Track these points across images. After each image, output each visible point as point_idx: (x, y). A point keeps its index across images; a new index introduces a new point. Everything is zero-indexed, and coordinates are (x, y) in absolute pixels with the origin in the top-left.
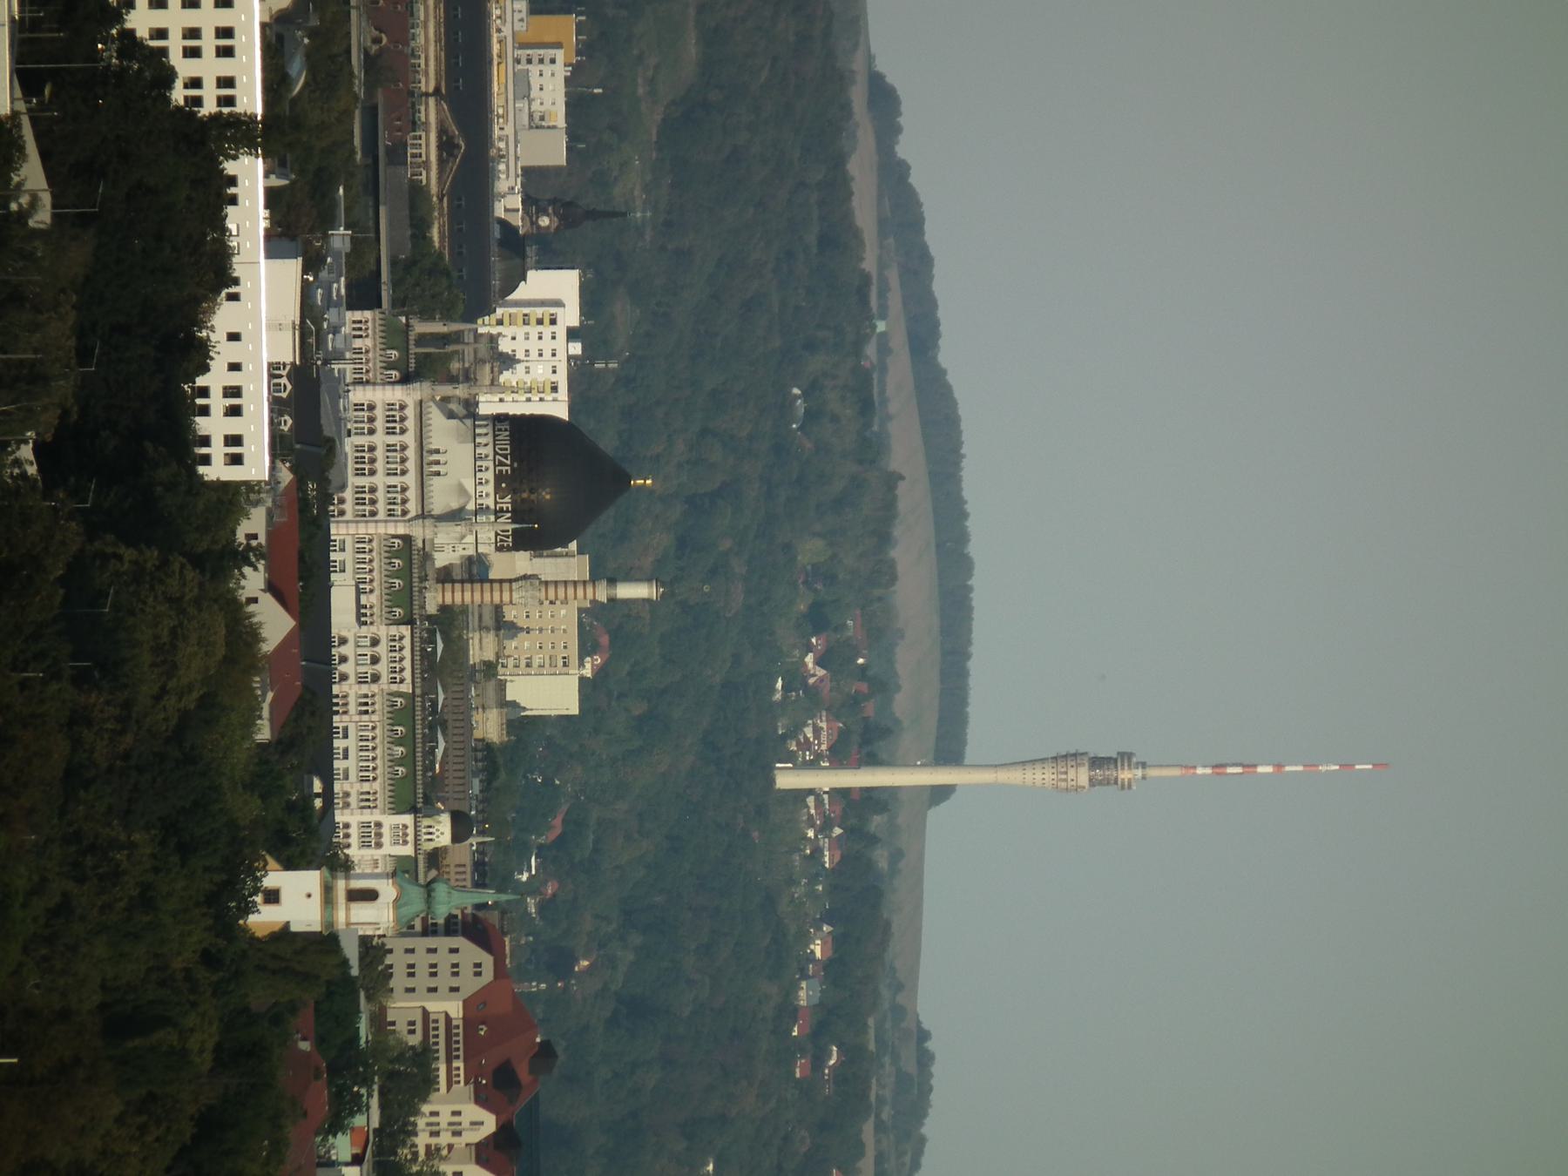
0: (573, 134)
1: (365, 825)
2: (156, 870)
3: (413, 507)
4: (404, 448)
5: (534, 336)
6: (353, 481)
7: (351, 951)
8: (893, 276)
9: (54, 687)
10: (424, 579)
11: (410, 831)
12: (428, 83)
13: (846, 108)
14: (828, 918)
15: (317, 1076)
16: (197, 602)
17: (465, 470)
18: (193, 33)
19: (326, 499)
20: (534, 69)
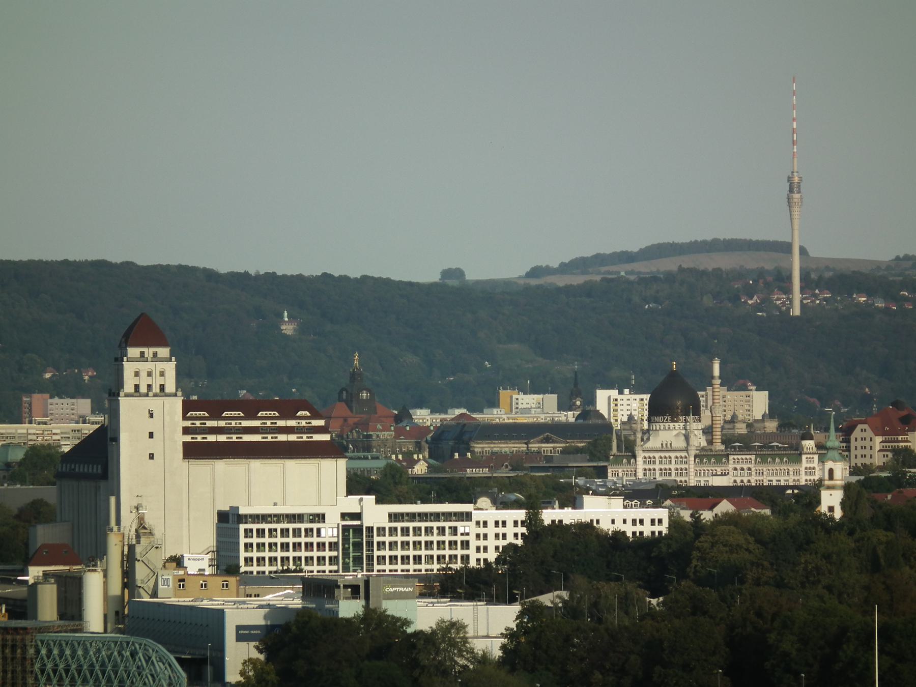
0: (544, 392)
1: (806, 473)
2: (816, 553)
3: (684, 454)
4: (661, 457)
5: (622, 407)
6: (673, 477)
7: (854, 479)
8: (603, 269)
9: (744, 591)
10: (711, 450)
11: (809, 456)
12: (523, 447)
13: (538, 287)
14: (850, 295)
15: (901, 492)
16: (713, 536)
17: (669, 434)
18: (497, 536)
19: (679, 487)
20: (520, 406)
